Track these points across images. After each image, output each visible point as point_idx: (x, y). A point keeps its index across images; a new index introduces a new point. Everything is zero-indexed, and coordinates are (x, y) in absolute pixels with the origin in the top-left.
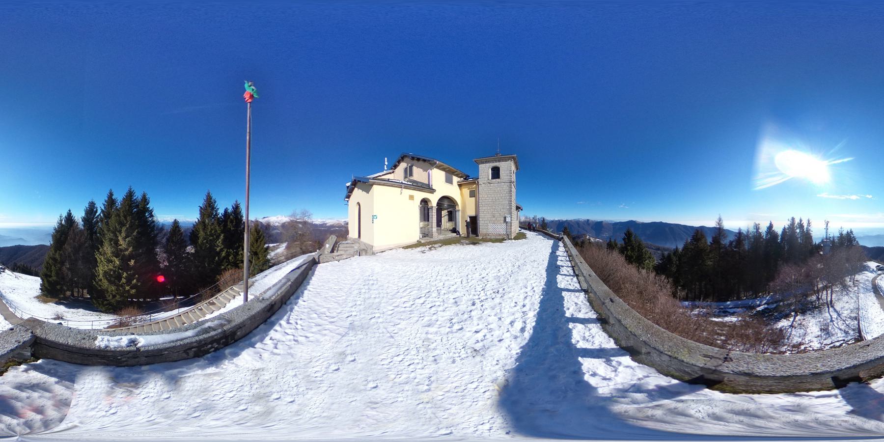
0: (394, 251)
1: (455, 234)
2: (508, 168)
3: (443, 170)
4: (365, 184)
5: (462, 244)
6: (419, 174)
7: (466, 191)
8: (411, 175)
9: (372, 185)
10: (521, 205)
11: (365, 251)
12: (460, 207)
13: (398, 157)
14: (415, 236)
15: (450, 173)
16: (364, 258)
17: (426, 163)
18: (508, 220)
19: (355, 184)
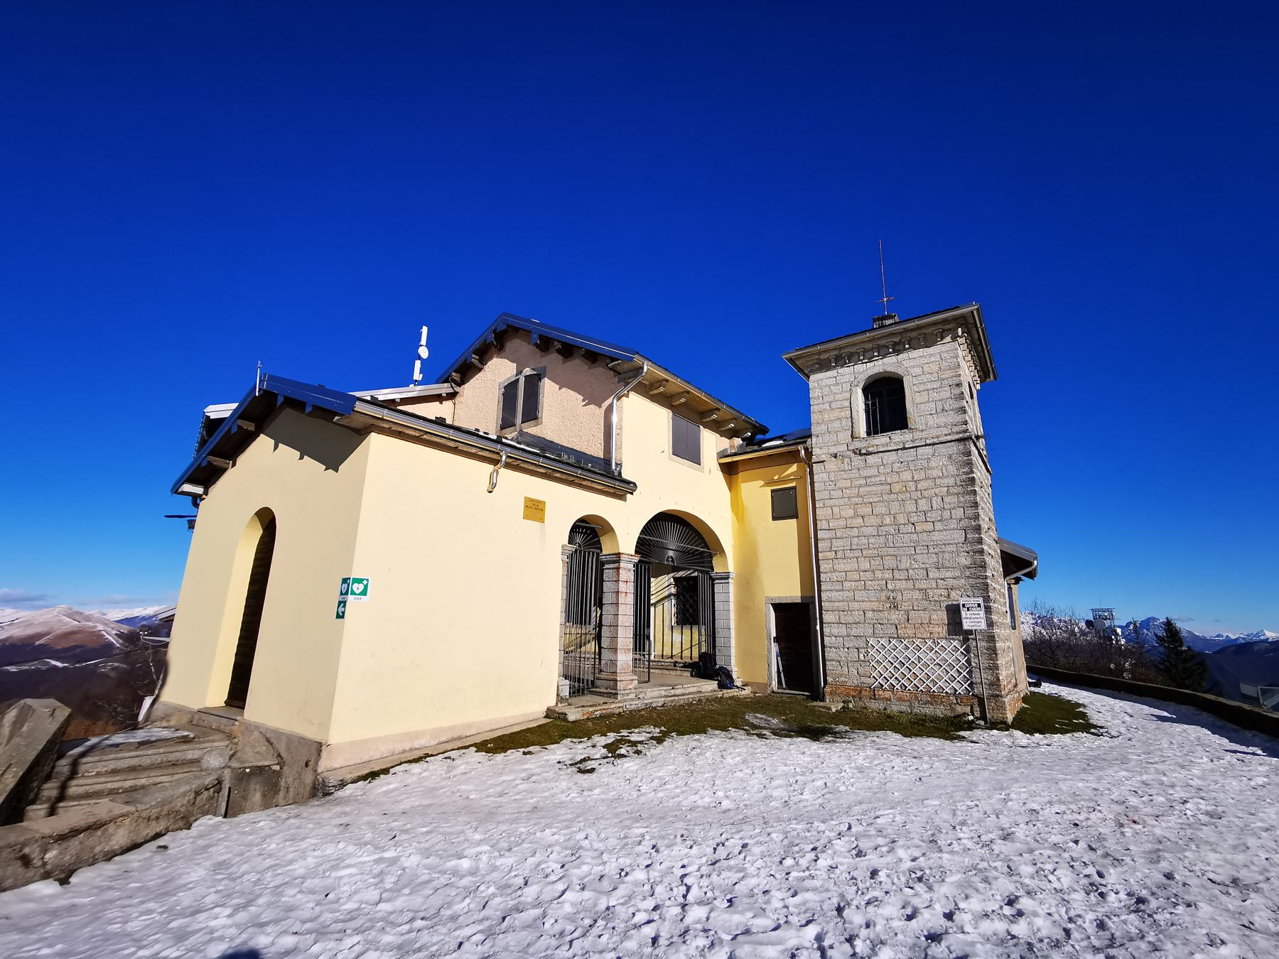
0: (436, 764)
1: (709, 686)
2: (939, 375)
3: (665, 400)
4: (329, 430)
5: (755, 731)
6: (564, 414)
7: (757, 492)
8: (532, 414)
9: (361, 433)
10: (1022, 544)
11: (286, 777)
12: (729, 562)
13: (480, 330)
14: (537, 689)
15: (690, 415)
16: (259, 823)
17: (599, 371)
18: (973, 620)
19: (261, 415)
